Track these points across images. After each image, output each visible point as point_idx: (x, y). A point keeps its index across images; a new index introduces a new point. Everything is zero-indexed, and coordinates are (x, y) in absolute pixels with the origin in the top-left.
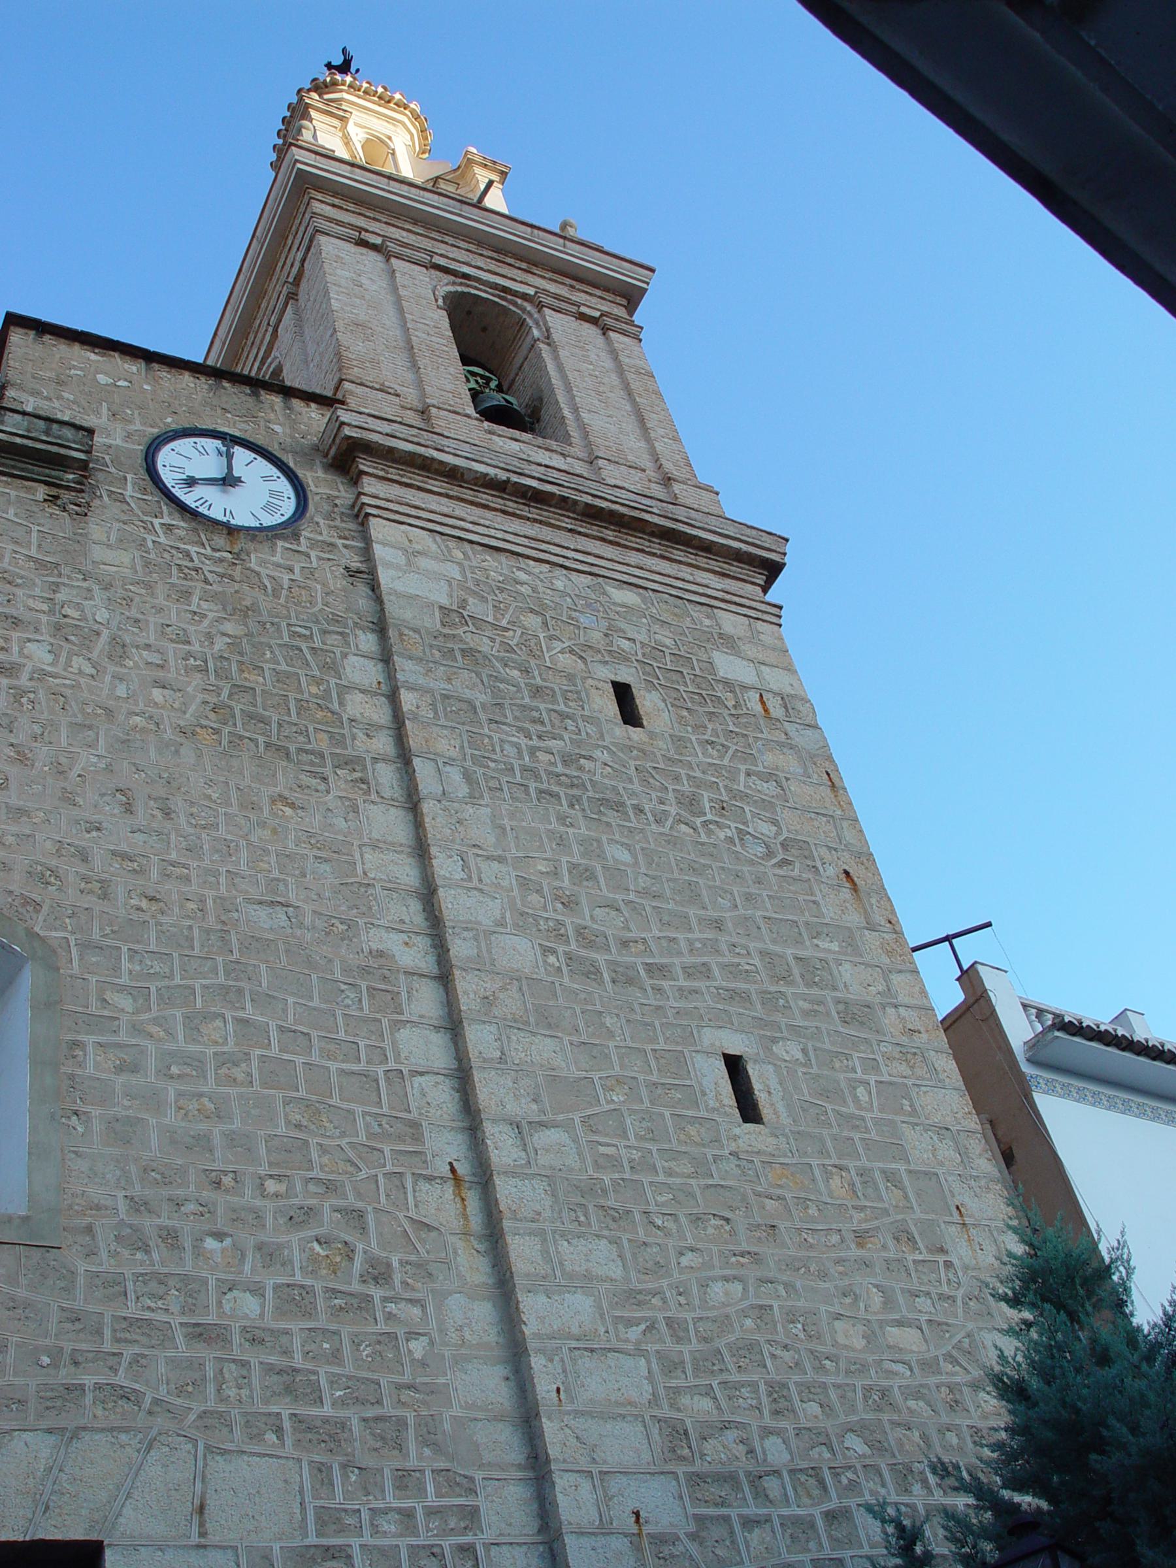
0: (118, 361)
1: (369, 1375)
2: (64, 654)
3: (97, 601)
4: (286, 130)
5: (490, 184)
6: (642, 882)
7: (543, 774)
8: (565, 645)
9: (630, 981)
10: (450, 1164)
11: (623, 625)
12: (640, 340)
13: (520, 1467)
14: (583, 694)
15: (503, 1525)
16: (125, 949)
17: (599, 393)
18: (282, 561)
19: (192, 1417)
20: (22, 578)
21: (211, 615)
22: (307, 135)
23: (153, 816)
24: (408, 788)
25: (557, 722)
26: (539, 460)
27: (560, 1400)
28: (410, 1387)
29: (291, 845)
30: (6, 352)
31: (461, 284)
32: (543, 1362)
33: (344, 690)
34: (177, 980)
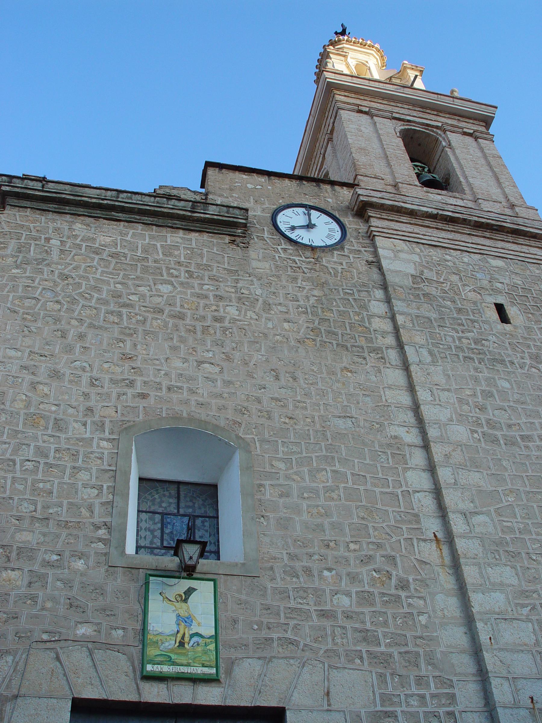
0: (255, 177)
1: (402, 632)
2: (243, 311)
3: (256, 286)
4: (320, 65)
5: (416, 76)
6: (516, 396)
7: (465, 349)
8: (471, 288)
9: (513, 444)
10: (434, 533)
11: (497, 277)
12: (493, 141)
13: (473, 675)
14: (481, 310)
15: (467, 702)
16: (280, 441)
17: (476, 169)
18: (337, 260)
19: (322, 652)
20: (222, 278)
21: (307, 287)
22: (330, 66)
23: (289, 381)
24: (403, 360)
25: (470, 324)
26: (451, 203)
27: (491, 643)
28: (420, 637)
29: (352, 390)
30: (207, 179)
31: (407, 125)
32: (482, 625)
33: (370, 317)
34: (304, 454)
